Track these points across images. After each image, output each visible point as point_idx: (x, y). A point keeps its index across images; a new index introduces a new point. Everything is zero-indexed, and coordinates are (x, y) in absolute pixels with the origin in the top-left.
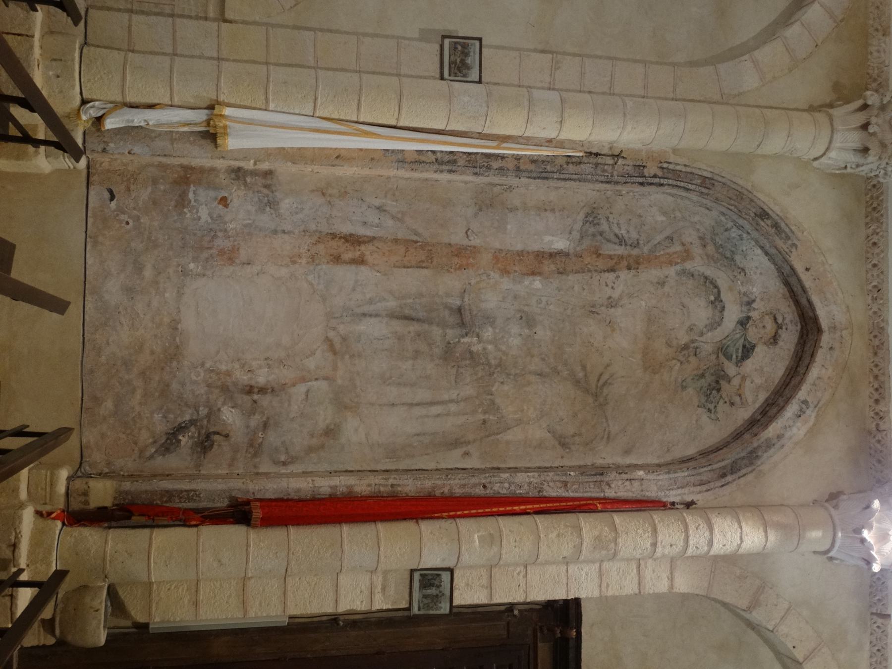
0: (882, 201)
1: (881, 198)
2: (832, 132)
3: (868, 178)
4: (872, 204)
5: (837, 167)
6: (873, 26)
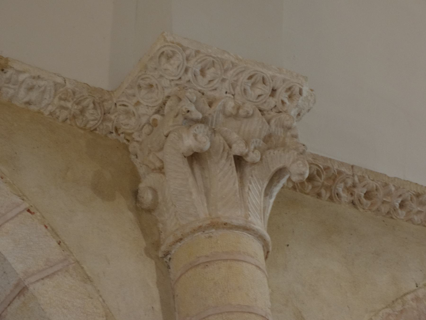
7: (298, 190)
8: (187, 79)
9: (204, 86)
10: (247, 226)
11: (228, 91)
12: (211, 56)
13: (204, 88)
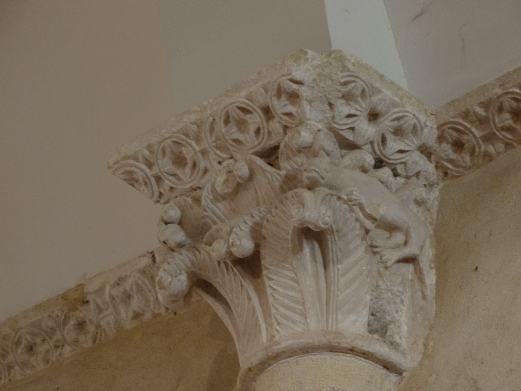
0: (486, 105)
1: (481, 111)
2: (277, 357)
3: (446, 174)
4: (509, 129)
5: (417, 286)
6: (76, 342)
7: (516, 144)
8: (167, 188)
9: (190, 180)
10: (270, 354)
11: (220, 160)
12: (165, 139)
13: (192, 181)
